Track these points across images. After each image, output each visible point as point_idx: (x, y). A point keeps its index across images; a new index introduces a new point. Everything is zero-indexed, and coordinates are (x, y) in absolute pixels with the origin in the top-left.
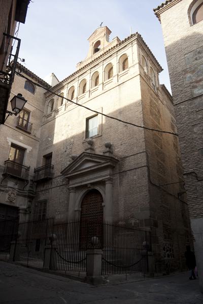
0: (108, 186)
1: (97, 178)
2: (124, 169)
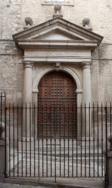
0: (87, 71)
1: (68, 57)
2: (105, 57)
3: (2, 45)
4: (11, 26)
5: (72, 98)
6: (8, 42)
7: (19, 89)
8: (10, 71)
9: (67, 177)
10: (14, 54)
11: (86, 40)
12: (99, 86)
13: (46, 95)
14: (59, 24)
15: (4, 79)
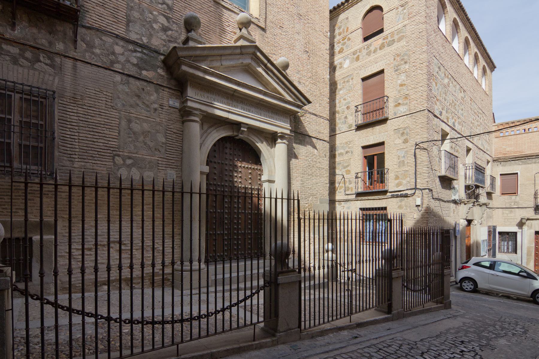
3: (129, 53)
6: (145, 51)
7: (171, 161)
9: (235, 329)
14: (254, 57)
15: (134, 133)
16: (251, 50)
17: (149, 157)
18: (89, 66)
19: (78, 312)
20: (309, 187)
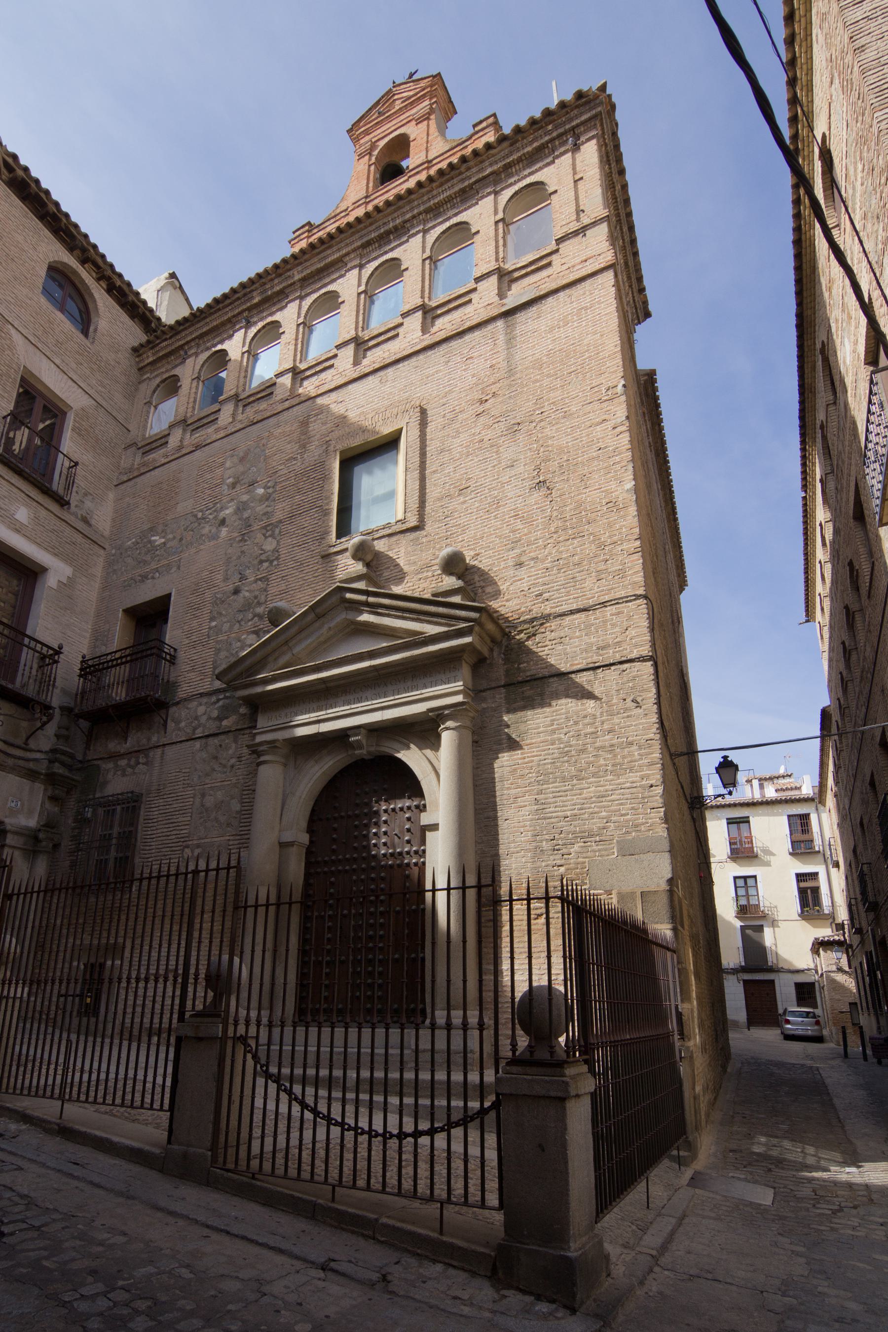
4: (239, 644)
5: (390, 851)
6: (227, 694)
8: (226, 783)
10: (239, 727)
11: (432, 630)
12: (509, 788)
13: (334, 851)
15: (207, 810)
16: (335, 599)
17: (219, 839)
18: (174, 746)
19: (337, 1124)
20: (569, 813)
